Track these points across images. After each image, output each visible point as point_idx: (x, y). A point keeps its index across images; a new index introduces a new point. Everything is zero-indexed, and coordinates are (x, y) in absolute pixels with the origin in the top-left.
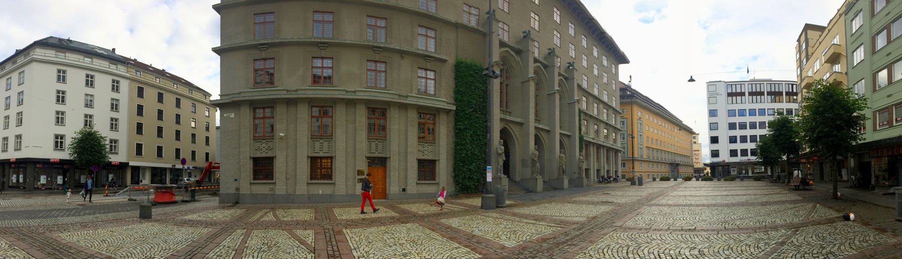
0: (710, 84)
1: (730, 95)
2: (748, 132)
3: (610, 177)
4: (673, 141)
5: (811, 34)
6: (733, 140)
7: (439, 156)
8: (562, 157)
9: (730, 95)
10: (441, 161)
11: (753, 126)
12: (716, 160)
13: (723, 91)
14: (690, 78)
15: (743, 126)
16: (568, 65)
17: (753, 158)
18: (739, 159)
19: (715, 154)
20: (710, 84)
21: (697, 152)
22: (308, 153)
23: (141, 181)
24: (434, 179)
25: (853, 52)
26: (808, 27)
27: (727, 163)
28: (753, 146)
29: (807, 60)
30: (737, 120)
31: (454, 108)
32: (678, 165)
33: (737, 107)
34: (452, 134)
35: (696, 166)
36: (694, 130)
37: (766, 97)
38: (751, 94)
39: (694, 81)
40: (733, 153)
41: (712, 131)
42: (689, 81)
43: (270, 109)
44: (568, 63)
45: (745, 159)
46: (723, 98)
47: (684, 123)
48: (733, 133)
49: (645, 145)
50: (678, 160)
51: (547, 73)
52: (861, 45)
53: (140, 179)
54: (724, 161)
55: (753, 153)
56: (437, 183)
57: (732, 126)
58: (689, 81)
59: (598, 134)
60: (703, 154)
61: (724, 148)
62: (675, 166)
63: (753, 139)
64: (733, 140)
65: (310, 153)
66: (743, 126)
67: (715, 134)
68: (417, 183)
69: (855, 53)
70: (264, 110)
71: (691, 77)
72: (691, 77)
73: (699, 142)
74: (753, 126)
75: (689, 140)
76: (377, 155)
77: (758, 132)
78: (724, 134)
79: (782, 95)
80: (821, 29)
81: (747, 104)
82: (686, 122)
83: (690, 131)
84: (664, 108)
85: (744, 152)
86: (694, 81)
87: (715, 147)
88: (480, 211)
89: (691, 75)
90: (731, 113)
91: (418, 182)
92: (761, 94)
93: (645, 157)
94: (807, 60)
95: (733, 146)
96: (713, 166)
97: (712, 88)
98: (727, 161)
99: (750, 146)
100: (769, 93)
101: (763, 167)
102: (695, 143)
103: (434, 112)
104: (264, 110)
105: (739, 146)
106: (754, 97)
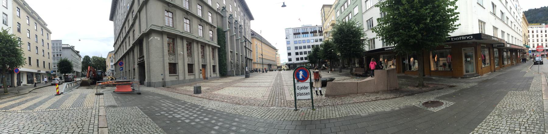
0: (286, 29)
1: (295, 34)
2: (303, 50)
3: (252, 70)
4: (268, 54)
5: (326, 9)
6: (297, 54)
9: (295, 34)
11: (305, 47)
12: (290, 62)
13: (291, 32)
15: (301, 48)
17: (306, 61)
18: (300, 61)
19: (290, 60)
20: (286, 29)
21: (278, 59)
23: (22, 82)
24: (176, 74)
25: (354, 9)
26: (324, 6)
27: (295, 63)
28: (306, 56)
29: (325, 21)
30: (298, 45)
32: (271, 65)
33: (298, 39)
34: (227, 55)
35: (278, 65)
36: (276, 48)
37: (310, 34)
38: (303, 33)
40: (298, 59)
41: (289, 51)
45: (302, 61)
46: (292, 36)
47: (272, 45)
48: (297, 51)
49: (259, 57)
50: (271, 63)
52: (357, 6)
53: (21, 81)
54: (294, 63)
55: (306, 59)
56: (177, 75)
57: (296, 48)
59: (203, 51)
60: (281, 59)
61: (294, 57)
62: (270, 65)
63: (305, 53)
64: (297, 54)
66: (301, 48)
67: (289, 51)
68: (170, 76)
69: (355, 9)
73: (279, 54)
74: (305, 47)
75: (275, 54)
76: (190, 63)
77: (307, 50)
78: (293, 52)
79: (317, 32)
80: (330, 6)
81: (301, 38)
82: (273, 44)
83: (274, 49)
84: (257, 33)
85: (302, 59)
87: (290, 57)
88: (272, 64)
90: (295, 42)
91: (170, 75)
92: (307, 33)
93: (259, 62)
94: (325, 21)
95: (297, 56)
96: (289, 65)
97: (287, 31)
98: (295, 63)
99: (304, 56)
100: (311, 33)
101: (311, 64)
102: (277, 54)
103: (215, 47)
105: (299, 56)
106: (304, 35)
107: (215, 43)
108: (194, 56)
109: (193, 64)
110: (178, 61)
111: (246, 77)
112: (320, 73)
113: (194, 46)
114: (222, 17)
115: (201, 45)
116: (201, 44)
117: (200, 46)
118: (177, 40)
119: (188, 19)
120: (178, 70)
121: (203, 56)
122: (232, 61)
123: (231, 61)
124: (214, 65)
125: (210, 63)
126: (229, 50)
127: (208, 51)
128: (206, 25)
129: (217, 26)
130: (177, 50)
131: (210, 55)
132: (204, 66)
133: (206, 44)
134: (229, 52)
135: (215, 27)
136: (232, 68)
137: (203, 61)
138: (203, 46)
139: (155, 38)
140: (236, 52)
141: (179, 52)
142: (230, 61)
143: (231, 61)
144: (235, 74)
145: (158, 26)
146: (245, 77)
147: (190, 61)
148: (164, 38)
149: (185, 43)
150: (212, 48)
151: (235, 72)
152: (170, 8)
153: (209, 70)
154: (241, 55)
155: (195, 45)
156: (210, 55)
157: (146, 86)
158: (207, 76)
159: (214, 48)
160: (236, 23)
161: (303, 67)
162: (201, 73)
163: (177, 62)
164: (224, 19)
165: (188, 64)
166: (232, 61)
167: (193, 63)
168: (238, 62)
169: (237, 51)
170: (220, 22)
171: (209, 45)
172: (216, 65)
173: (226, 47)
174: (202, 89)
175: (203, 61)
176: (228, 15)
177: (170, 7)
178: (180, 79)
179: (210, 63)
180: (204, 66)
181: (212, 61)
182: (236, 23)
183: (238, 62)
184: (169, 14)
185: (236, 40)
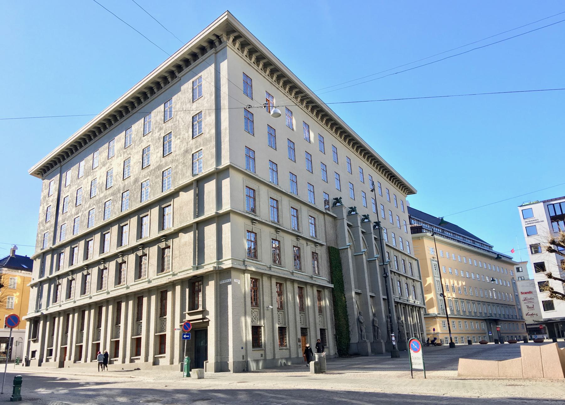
31: (332, 286)
44: (364, 216)
103: (324, 287)
107: (324, 280)
109: (285, 328)
111: (392, 357)
112: (246, 209)
113: (308, 290)
116: (251, 274)
123: (358, 319)
125: (315, 324)
129: (326, 242)
133: (306, 284)
136: (361, 336)
138: (281, 285)
140: (369, 294)
142: (356, 317)
143: (358, 319)
144: (369, 350)
146: (391, 357)
148: (314, 289)
151: (369, 345)
154: (371, 297)
155: (289, 285)
159: (321, 289)
161: (354, 246)
162: (300, 345)
164: (339, 222)
169: (372, 291)
170: (331, 231)
178: (300, 356)
179: (315, 324)
185: (379, 265)
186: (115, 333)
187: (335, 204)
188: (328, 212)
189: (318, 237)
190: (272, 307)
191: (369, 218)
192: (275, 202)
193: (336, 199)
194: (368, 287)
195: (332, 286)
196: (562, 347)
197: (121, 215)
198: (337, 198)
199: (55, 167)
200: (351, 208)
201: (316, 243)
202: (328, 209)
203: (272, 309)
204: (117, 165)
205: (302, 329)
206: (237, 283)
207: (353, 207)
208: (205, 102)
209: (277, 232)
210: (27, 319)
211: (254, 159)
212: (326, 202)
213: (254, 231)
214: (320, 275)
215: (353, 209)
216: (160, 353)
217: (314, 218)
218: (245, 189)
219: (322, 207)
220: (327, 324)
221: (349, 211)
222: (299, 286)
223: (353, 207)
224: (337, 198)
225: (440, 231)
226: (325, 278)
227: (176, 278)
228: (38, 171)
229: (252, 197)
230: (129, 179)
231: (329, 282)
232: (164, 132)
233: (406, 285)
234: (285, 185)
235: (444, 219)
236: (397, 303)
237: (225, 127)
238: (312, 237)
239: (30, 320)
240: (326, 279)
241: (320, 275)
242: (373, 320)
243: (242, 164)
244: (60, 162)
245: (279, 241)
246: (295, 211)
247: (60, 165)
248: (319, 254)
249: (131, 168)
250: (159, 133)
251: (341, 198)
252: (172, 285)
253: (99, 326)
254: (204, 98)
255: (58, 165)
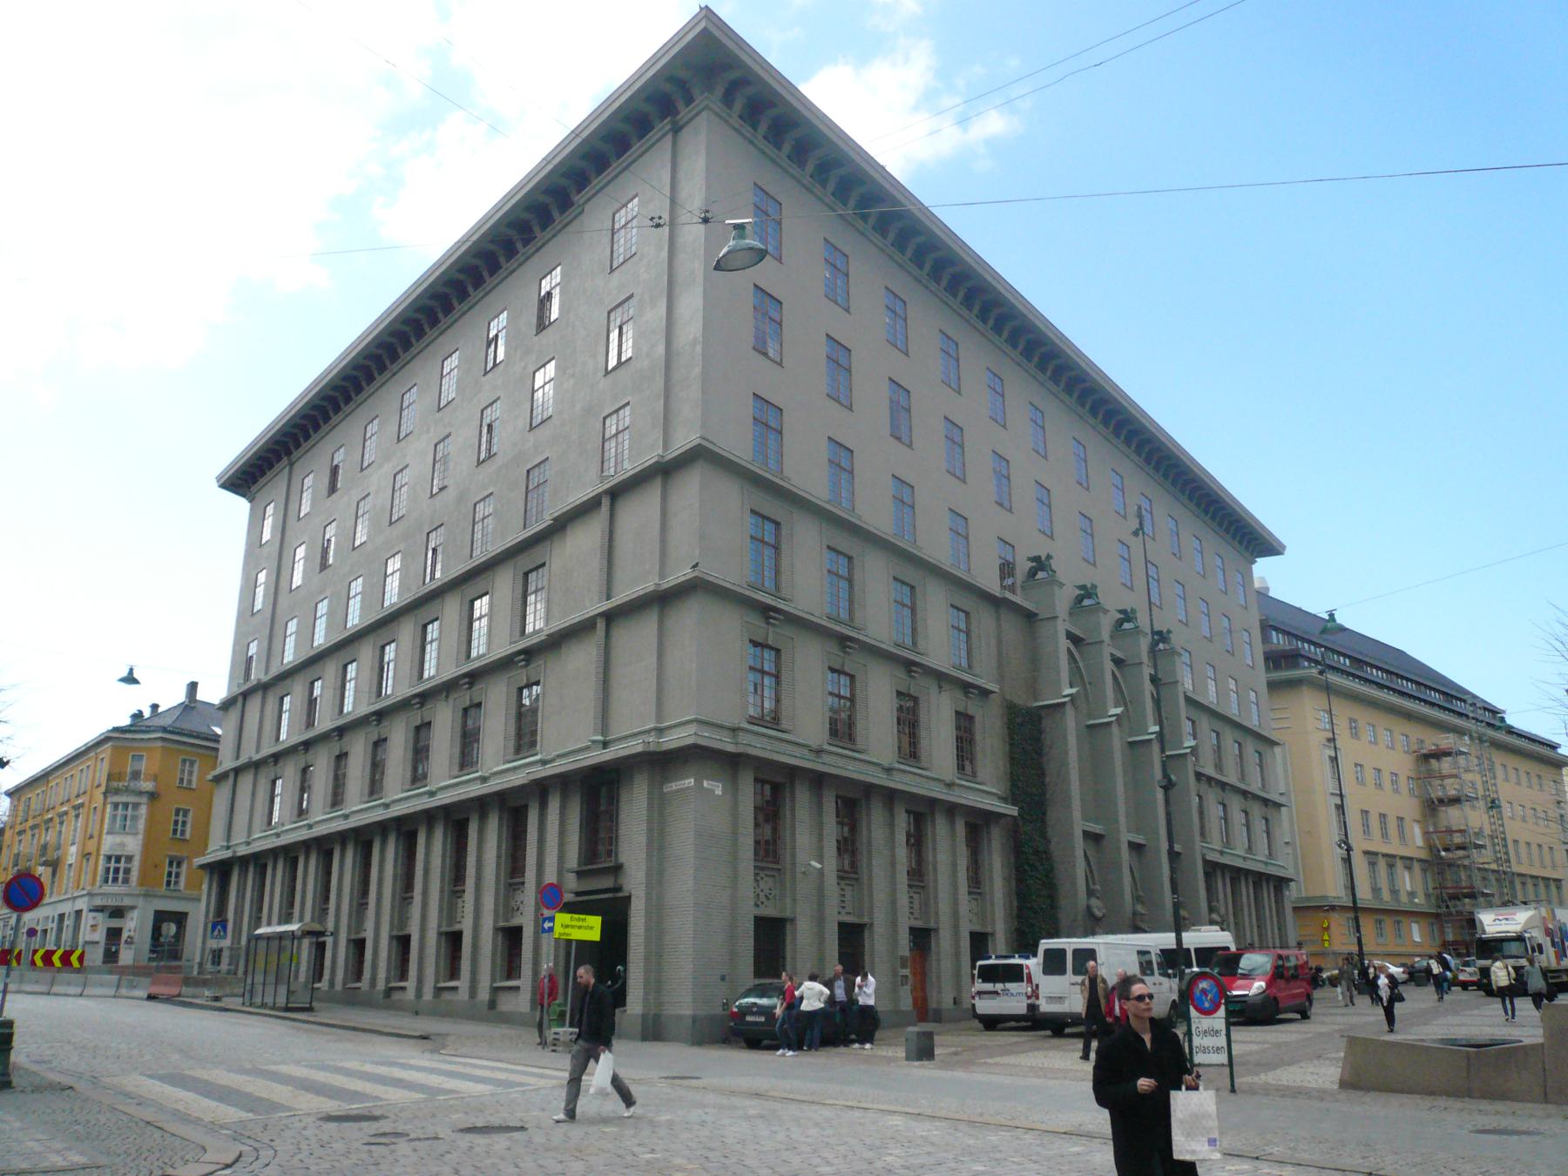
7: (871, 913)
8: (1523, 967)
10: (941, 931)
14: (125, 674)
16: (1078, 592)
22: (439, 926)
31: (1013, 811)
39: (135, 681)
42: (123, 680)
43: (910, 1008)
44: (1121, 612)
51: (1125, 681)
58: (123, 680)
65: (444, 924)
70: (1032, 1008)
71: (131, 670)
72: (131, 670)
86: (135, 681)
89: (132, 663)
103: (989, 817)
104: (1032, 1008)
108: (870, 877)
110: (937, 922)
113: (938, 831)
114: (1030, 617)
115: (756, 780)
117: (830, 806)
118: (797, 792)
119: (771, 648)
120: (794, 959)
121: (918, 875)
122: (1094, 902)
123: (1089, 908)
124: (978, 928)
126: (1079, 825)
127: (947, 847)
128: (934, 689)
129: (1001, 680)
130: (794, 848)
131: (954, 865)
132: (922, 938)
134: (1125, 847)
135: (985, 693)
137: (848, 897)
139: (705, 784)
140: (1126, 837)
141: (801, 857)
145: (721, 727)
147: (849, 909)
149: (902, 821)
150: (908, 812)
152: (771, 629)
153: (946, 965)
156: (954, 865)
157: (684, 1041)
158: (939, 1002)
159: (978, 823)
160: (1161, 646)
163: (788, 914)
165: (841, 925)
166: (1094, 902)
167: (866, 920)
168: (1139, 908)
171: (952, 810)
172: (989, 930)
173: (1053, 815)
174: (1340, 1070)
175: (916, 905)
176: (1063, 600)
177: (774, 625)
180: (922, 938)
181: (965, 902)
182: (1161, 646)
183: (1139, 908)
184: (763, 658)
186: (401, 915)
187: (1032, 574)
188: (1009, 595)
189: (977, 670)
190: (819, 866)
191: (1136, 619)
192: (906, 590)
193: (1037, 559)
194: (1122, 820)
195: (1013, 811)
196: (1153, 1041)
197: (422, 593)
198: (1040, 557)
199: (278, 467)
200: (1083, 587)
201: (966, 687)
202: (1012, 589)
203: (821, 872)
204: (417, 452)
205: (913, 931)
206: (713, 791)
207: (1165, 631)
208: (644, 269)
209: (843, 648)
210: (202, 867)
211: (851, 472)
212: (1007, 569)
213: (846, 669)
214: (979, 780)
215: (1087, 592)
216: (509, 977)
217: (912, 588)
218: (750, 520)
219: (990, 581)
220: (993, 921)
221: (1117, 621)
222: (840, 793)
223: (1089, 586)
224: (1040, 557)
225: (1347, 661)
226: (994, 787)
227: (549, 770)
228: (240, 479)
229: (767, 544)
230: (444, 493)
231: (1004, 799)
232: (534, 359)
233: (1264, 822)
234: (877, 514)
235: (1341, 619)
236: (1212, 869)
237: (691, 337)
238: (959, 668)
239: (210, 868)
240: (994, 790)
241: (979, 780)
242: (1135, 913)
243: (738, 444)
244: (289, 453)
245: (852, 677)
246: (962, 615)
247: (290, 460)
248: (978, 719)
249: (451, 465)
250: (523, 364)
251: (1049, 557)
252: (541, 789)
253: (365, 892)
254: (640, 260)
255: (285, 460)
